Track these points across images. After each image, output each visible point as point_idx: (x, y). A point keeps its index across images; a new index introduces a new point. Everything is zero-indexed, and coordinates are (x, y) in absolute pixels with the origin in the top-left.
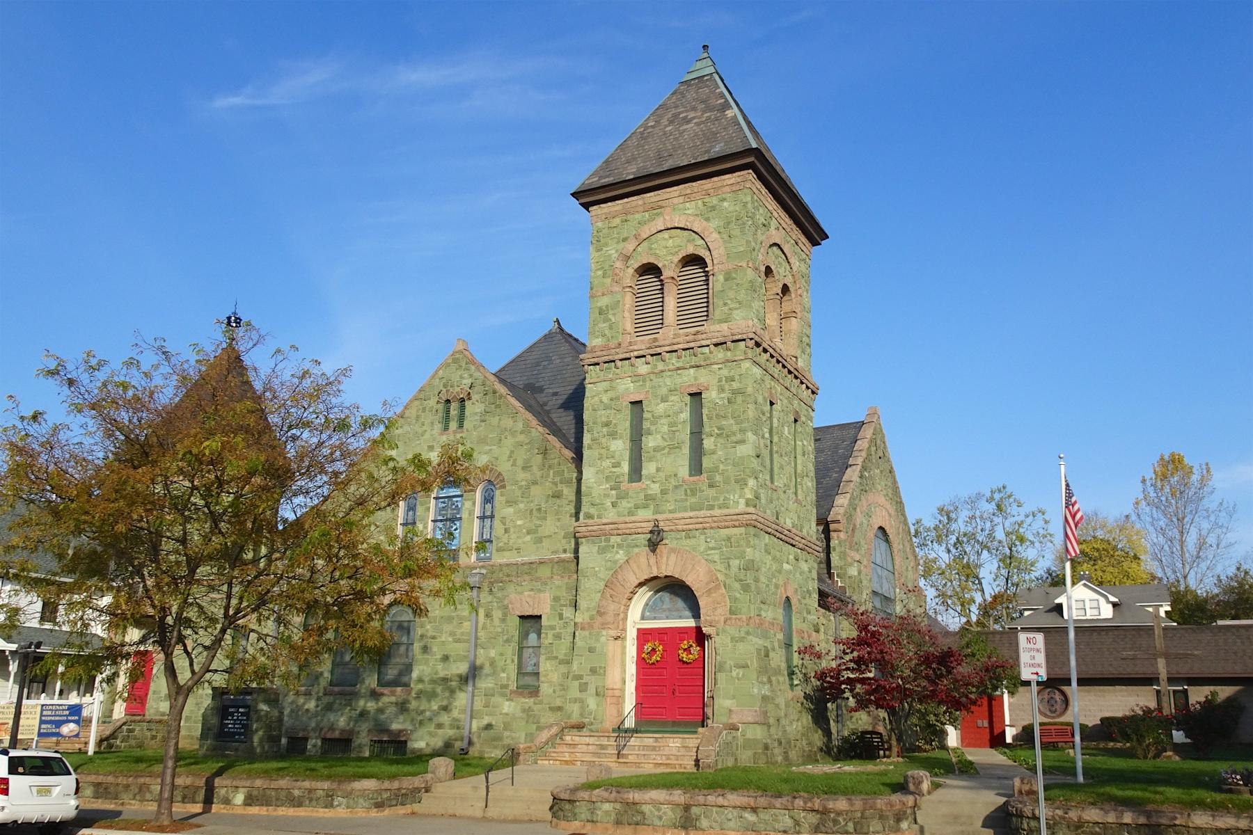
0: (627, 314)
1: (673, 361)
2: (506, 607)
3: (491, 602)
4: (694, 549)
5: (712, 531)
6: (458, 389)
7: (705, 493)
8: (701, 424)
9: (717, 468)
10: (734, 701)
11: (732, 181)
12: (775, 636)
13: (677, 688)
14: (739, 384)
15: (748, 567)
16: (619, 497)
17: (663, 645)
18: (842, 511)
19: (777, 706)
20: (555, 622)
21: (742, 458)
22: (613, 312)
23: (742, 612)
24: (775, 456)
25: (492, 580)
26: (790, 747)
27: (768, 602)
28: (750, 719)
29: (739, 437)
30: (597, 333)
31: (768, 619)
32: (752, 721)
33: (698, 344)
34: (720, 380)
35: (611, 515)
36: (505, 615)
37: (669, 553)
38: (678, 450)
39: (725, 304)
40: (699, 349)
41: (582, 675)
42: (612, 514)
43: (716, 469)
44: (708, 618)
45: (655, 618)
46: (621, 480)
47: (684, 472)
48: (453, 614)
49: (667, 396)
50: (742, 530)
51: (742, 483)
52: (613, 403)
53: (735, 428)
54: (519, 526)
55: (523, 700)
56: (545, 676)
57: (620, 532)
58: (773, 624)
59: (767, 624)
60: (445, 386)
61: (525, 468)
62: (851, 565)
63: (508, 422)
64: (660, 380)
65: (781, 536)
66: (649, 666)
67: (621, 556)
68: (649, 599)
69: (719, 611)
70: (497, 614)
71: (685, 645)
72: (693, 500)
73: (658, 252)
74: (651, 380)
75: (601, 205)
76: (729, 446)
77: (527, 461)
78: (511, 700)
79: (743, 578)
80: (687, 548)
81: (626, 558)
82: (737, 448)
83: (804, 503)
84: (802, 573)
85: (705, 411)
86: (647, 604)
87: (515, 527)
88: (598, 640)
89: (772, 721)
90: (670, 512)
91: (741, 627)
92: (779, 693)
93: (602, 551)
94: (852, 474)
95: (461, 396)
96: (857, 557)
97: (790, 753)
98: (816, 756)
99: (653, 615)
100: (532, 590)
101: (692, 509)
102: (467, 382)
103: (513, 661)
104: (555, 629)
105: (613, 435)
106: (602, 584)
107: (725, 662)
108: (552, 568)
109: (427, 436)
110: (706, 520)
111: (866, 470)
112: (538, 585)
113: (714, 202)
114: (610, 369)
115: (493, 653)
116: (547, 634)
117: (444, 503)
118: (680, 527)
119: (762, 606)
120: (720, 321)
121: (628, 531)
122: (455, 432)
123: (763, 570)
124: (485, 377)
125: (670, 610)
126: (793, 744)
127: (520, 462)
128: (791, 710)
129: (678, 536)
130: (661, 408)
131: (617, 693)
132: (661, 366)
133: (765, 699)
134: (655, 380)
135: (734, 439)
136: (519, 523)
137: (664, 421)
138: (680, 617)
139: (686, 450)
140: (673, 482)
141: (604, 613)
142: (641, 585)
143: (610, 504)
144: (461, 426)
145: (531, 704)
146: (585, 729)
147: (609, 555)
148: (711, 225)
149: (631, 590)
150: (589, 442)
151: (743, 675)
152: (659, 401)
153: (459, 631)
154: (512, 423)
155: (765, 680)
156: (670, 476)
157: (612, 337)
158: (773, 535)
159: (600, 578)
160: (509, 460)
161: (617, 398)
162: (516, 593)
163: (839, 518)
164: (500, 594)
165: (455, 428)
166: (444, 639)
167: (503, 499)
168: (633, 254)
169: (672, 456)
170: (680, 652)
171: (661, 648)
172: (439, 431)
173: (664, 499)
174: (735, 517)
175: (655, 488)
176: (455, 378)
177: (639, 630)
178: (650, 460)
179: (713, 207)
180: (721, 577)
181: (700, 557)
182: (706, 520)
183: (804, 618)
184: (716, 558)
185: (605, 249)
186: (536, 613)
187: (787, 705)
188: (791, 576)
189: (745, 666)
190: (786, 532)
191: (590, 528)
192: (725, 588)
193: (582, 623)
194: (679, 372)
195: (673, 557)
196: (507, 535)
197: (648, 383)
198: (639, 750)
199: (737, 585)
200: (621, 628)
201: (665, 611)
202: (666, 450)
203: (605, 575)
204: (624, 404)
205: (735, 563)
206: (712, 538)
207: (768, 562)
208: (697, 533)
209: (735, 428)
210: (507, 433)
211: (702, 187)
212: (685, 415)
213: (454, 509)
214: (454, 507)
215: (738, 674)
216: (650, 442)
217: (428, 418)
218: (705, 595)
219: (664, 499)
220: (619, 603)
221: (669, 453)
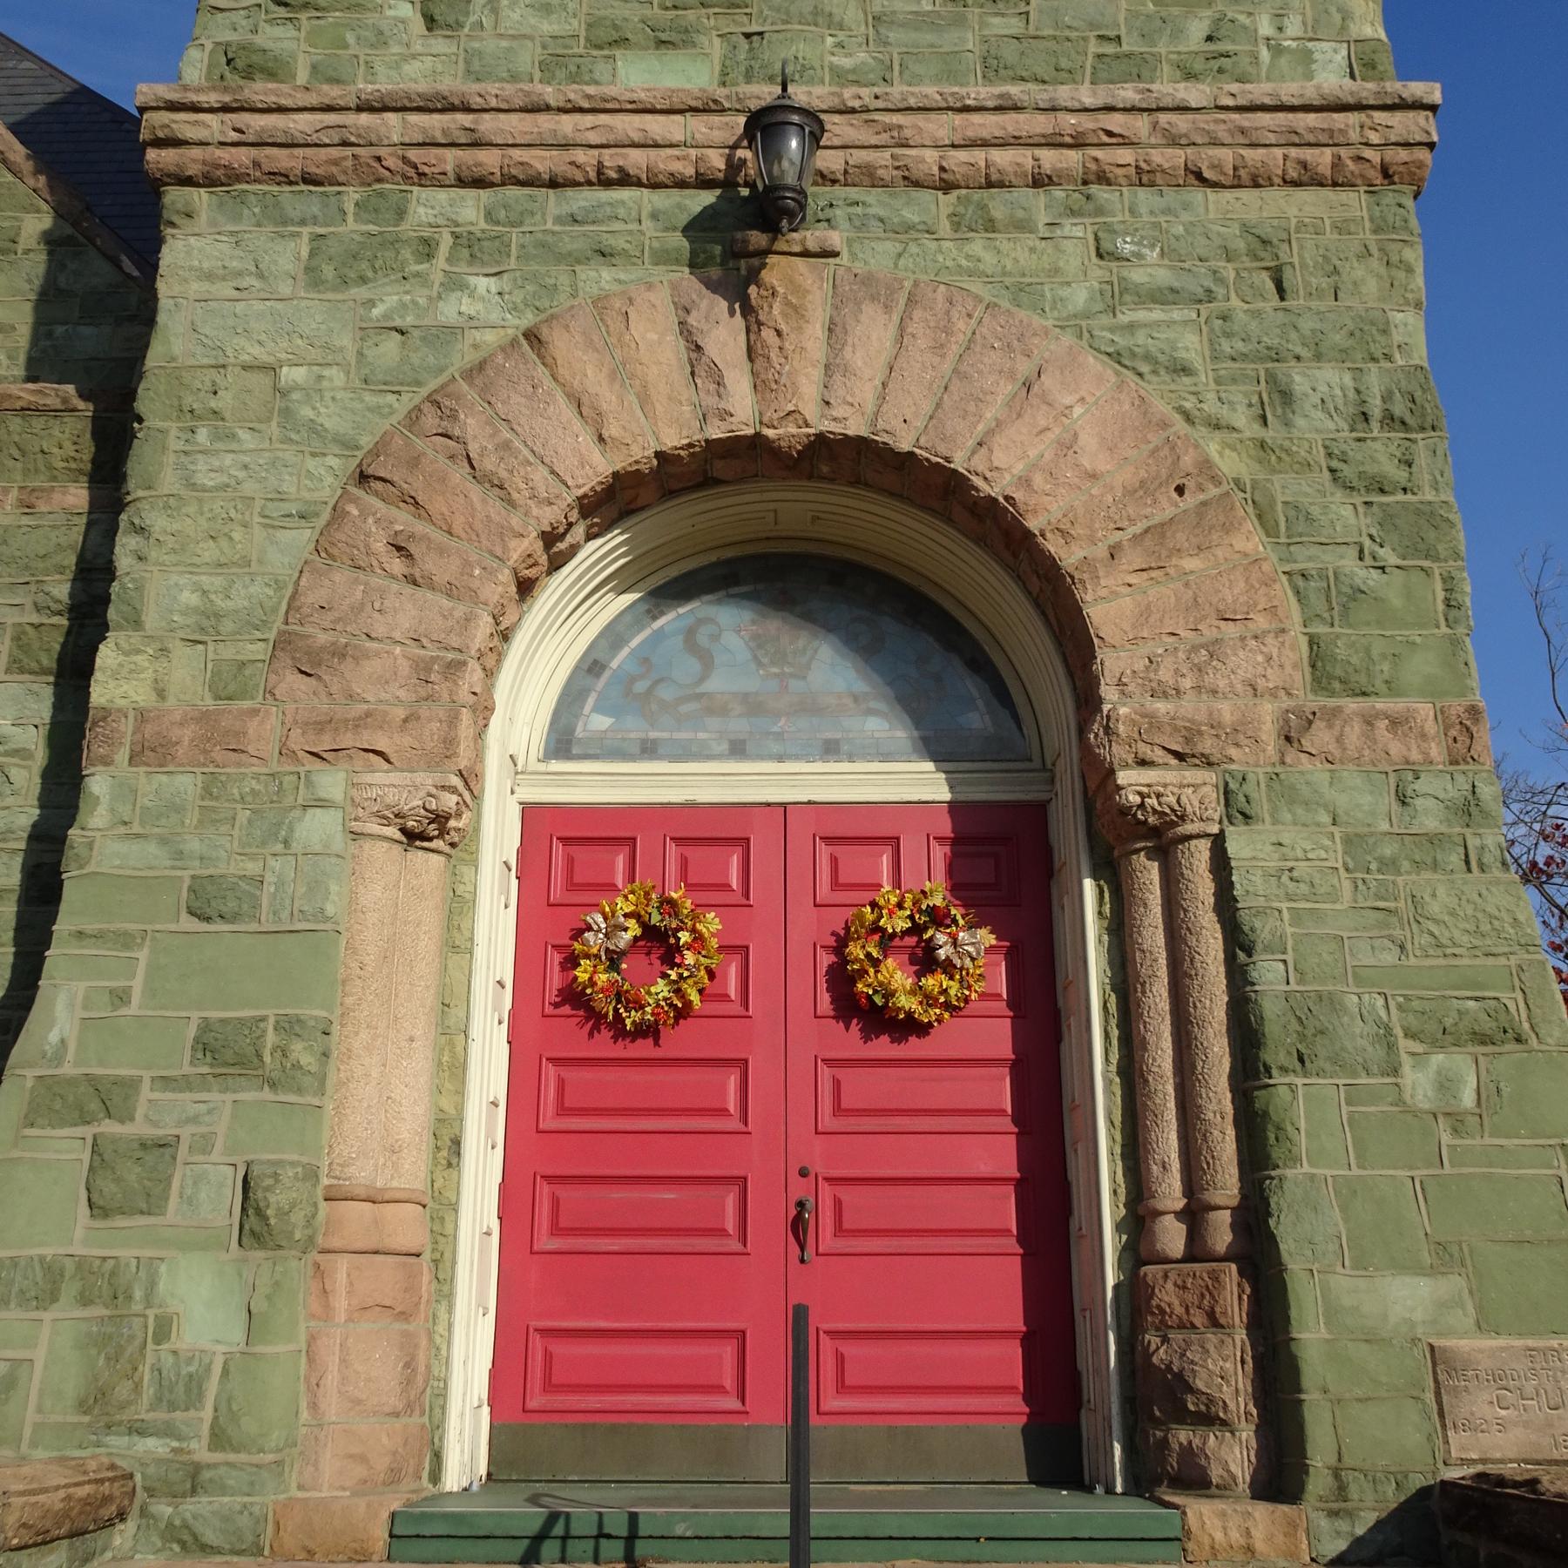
4: (1023, 291)
10: (1454, 1284)
17: (1139, 822)
41: (132, 1085)
45: (649, 750)
50: (1354, 202)
57: (489, 160)
69: (1243, 663)
86: (591, 666)
99: (635, 728)
110: (1116, 122)
118: (927, 161)
121: (542, 162)
125: (753, 706)
129: (911, 215)
131: (406, 1227)
138: (830, 750)
147: (388, 300)
159: (314, 429)
182: (1116, 122)
184: (1191, 347)
192: (1270, 530)
193: (142, 716)
201: (723, 711)
208: (1038, 204)
215: (1446, 1084)
218: (1133, 558)
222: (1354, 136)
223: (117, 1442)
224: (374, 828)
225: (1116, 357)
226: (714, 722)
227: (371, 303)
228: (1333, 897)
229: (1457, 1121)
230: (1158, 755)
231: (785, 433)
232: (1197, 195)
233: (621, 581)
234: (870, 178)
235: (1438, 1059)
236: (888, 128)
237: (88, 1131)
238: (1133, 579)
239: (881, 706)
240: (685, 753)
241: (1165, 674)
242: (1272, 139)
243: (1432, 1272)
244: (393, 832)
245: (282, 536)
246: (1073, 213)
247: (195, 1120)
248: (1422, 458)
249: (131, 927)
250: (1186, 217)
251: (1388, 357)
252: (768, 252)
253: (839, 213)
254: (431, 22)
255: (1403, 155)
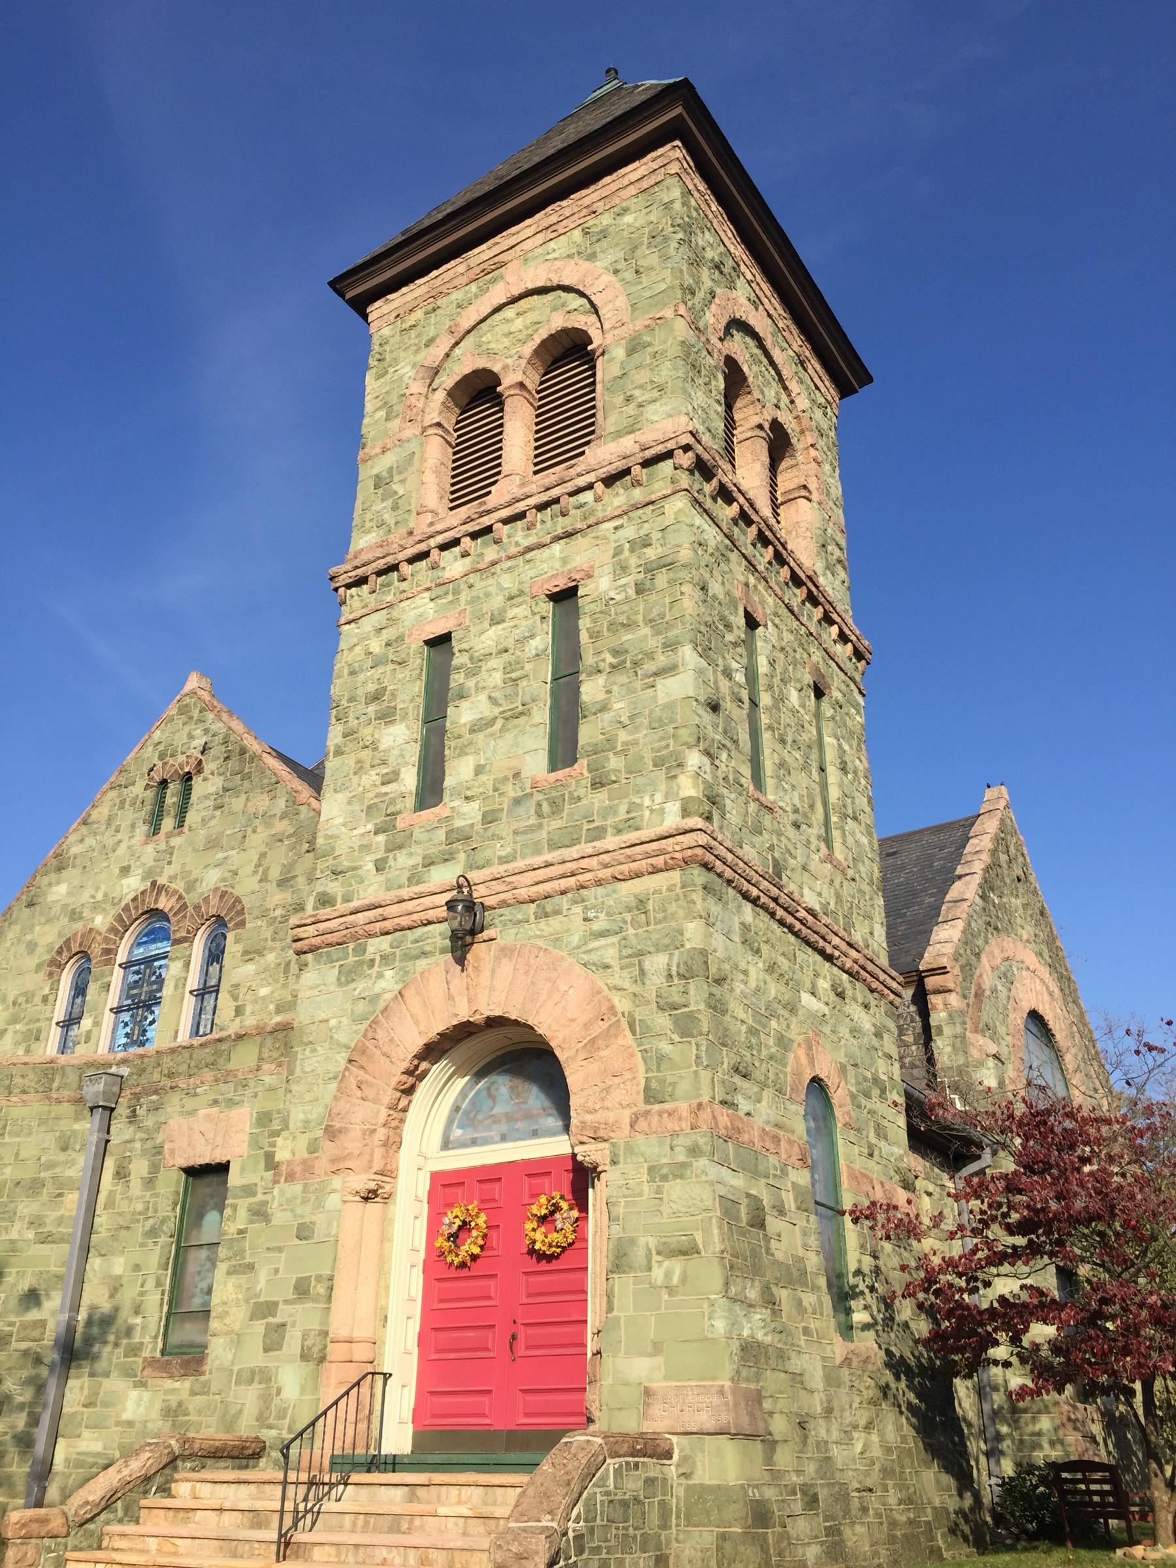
0: (430, 478)
1: (517, 536)
2: (158, 1150)
3: (129, 1142)
4: (556, 941)
5: (600, 890)
6: (181, 758)
7: (584, 802)
8: (575, 655)
9: (611, 741)
10: (660, 1360)
11: (643, 171)
12: (784, 1173)
13: (521, 1332)
14: (660, 550)
15: (689, 969)
16: (394, 847)
18: (949, 949)
19: (797, 1379)
20: (259, 1176)
21: (670, 706)
22: (400, 477)
23: (679, 1092)
24: (766, 736)
25: (138, 1090)
26: (847, 1512)
27: (758, 1075)
28: (705, 1420)
29: (662, 660)
30: (368, 525)
31: (759, 1121)
32: (710, 1425)
33: (569, 487)
34: (618, 552)
35: (372, 890)
36: (155, 1168)
37: (498, 959)
38: (523, 719)
39: (628, 399)
40: (573, 500)
41: (276, 1304)
42: (375, 886)
43: (610, 742)
44: (589, 1118)
45: (474, 1142)
46: (398, 807)
47: (536, 764)
48: (42, 1175)
49: (503, 611)
50: (675, 876)
51: (671, 764)
52: (391, 650)
53: (653, 643)
54: (263, 998)
55: (169, 1384)
56: (220, 1317)
57: (388, 925)
58: (776, 1140)
59: (756, 1134)
60: (162, 756)
61: (283, 883)
62: (980, 1064)
63: (261, 802)
64: (491, 581)
65: (790, 920)
66: (453, 1273)
67: (387, 982)
68: (463, 1094)
69: (617, 1096)
70: (139, 1168)
71: (540, 1207)
72: (556, 824)
73: (492, 345)
74: (470, 587)
75: (390, 297)
76: (638, 685)
77: (288, 868)
78: (142, 1384)
79: (677, 998)
80: (540, 943)
81: (399, 987)
82: (659, 686)
83: (850, 873)
84: (855, 1031)
85: (584, 623)
86: (456, 1109)
87: (255, 1002)
88: (320, 1205)
89: (779, 1426)
90: (503, 860)
91: (674, 1134)
92: (802, 1340)
93: (348, 976)
94: (966, 889)
95: (187, 770)
96: (993, 1048)
97: (847, 1532)
98: (932, 1539)
99: (471, 1134)
100: (216, 1102)
101: (553, 846)
102: (199, 742)
103: (159, 1284)
104: (254, 1194)
105: (387, 717)
106: (342, 1058)
107: (632, 1241)
108: (261, 1045)
109: (122, 850)
110: (584, 863)
111: (992, 889)
112: (228, 1089)
113: (605, 223)
114: (389, 585)
115: (119, 1266)
116: (235, 1208)
117: (137, 973)
118: (523, 893)
119: (737, 1080)
120: (618, 434)
121: (405, 921)
122: (169, 835)
123: (739, 987)
124: (230, 729)
125: (509, 1118)
126: (855, 1504)
127: (275, 873)
128: (843, 1396)
129: (520, 917)
130: (488, 638)
132: (491, 553)
133: (751, 1352)
134: (479, 585)
135: (650, 667)
136: (264, 992)
137: (496, 663)
138: (535, 1134)
139: (542, 715)
140: (511, 791)
141: (340, 1131)
142: (432, 1051)
143: (371, 866)
144: (181, 824)
145: (184, 1395)
146: (263, 1462)
148: (598, 264)
149: (405, 1065)
150: (339, 740)
151: (684, 1279)
152: (486, 624)
153: (52, 1215)
154: (267, 803)
155: (753, 1294)
156: (506, 779)
157: (397, 523)
158: (764, 907)
160: (255, 872)
161: (400, 639)
162: (182, 1114)
163: (944, 961)
164: (149, 1122)
165: (170, 828)
166: (14, 1235)
167: (239, 948)
168: (446, 365)
169: (509, 736)
170: (529, 1226)
171: (483, 1217)
172: (143, 838)
173: (490, 833)
174: (654, 846)
175: (470, 813)
176: (180, 739)
177: (435, 1176)
178: (462, 752)
179: (602, 231)
180: (622, 1004)
181: (570, 960)
182: (584, 863)
183: (871, 1147)
185: (391, 370)
186: (219, 1157)
187: (831, 1379)
188: (827, 1030)
189: (688, 1251)
190: (802, 914)
191: (322, 926)
192: (634, 1033)
194: (528, 556)
195: (506, 967)
196: (238, 1019)
197: (465, 596)
198: (353, 1531)
199: (663, 1021)
200: (377, 1165)
201: (497, 1121)
202: (499, 723)
203: (348, 1034)
204: (414, 647)
205: (657, 963)
206: (599, 908)
207: (753, 971)
208: (564, 901)
209: (653, 643)
210: (257, 822)
211: (580, 203)
212: (543, 640)
213: (154, 983)
214: (154, 978)
215: (668, 1275)
216: (461, 715)
217: (128, 816)
219: (490, 833)
220: (375, 1101)
221: (503, 729)
222: (670, 849)
223: (264, 1431)
224: (350, 1198)
225: (584, 965)
226: (495, 1127)
227: (355, 989)
228: (641, 1194)
229: (671, 1290)
230: (585, 1139)
231: (477, 1018)
232: (619, 885)
233: (458, 1072)
234: (504, 904)
235: (666, 1263)
236: (510, 883)
237: (264, 1321)
238: (583, 1063)
239: (554, 1112)
240: (486, 1142)
241: (590, 1105)
242: (640, 857)
243: (651, 1355)
244: (358, 1199)
245: (330, 1086)
246: (576, 903)
247: (291, 1315)
248: (692, 992)
249: (281, 1244)
250: (615, 896)
251: (683, 946)
252: (472, 944)
253: (496, 921)
254: (377, 870)
255: (689, 852)
